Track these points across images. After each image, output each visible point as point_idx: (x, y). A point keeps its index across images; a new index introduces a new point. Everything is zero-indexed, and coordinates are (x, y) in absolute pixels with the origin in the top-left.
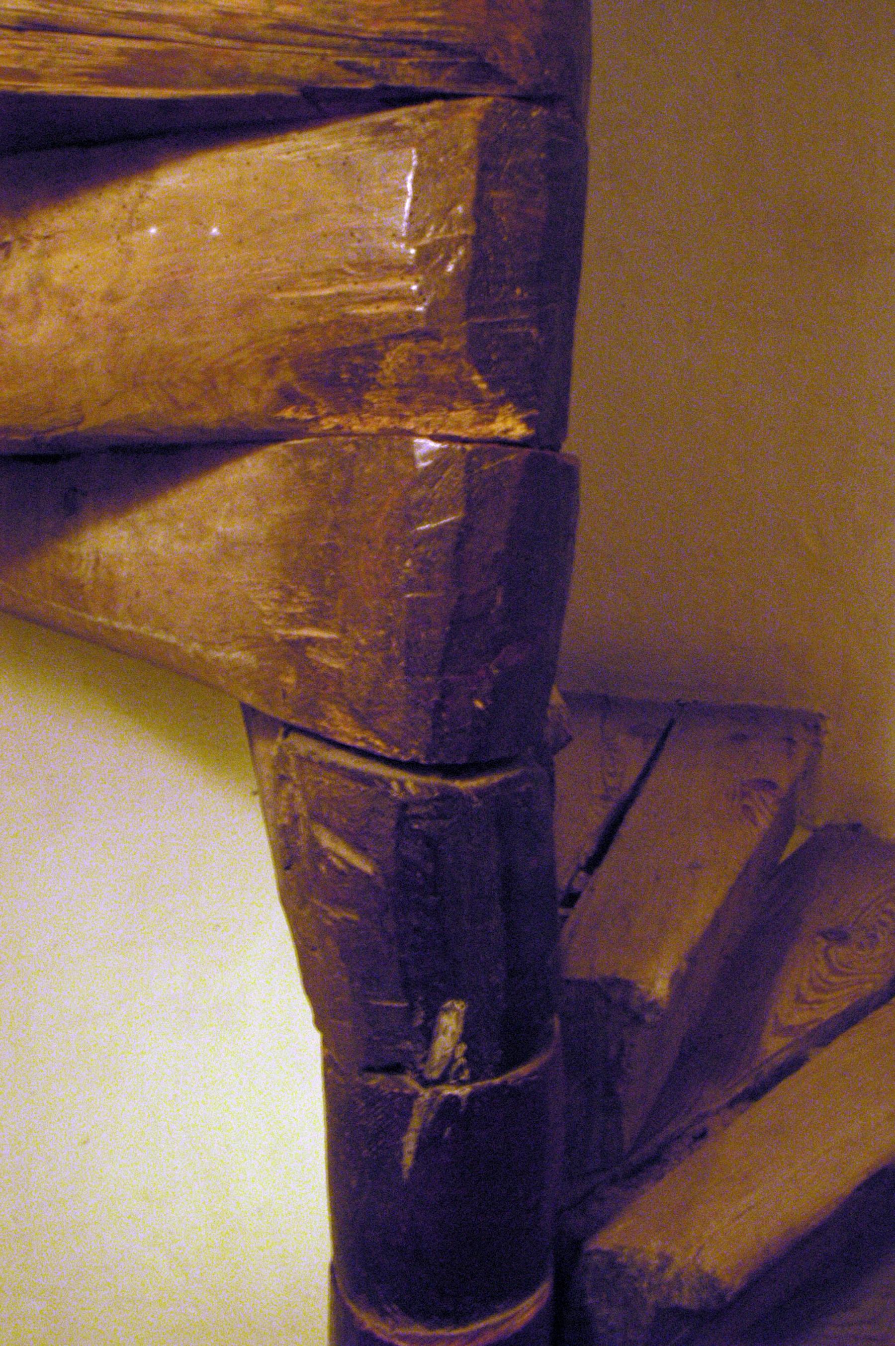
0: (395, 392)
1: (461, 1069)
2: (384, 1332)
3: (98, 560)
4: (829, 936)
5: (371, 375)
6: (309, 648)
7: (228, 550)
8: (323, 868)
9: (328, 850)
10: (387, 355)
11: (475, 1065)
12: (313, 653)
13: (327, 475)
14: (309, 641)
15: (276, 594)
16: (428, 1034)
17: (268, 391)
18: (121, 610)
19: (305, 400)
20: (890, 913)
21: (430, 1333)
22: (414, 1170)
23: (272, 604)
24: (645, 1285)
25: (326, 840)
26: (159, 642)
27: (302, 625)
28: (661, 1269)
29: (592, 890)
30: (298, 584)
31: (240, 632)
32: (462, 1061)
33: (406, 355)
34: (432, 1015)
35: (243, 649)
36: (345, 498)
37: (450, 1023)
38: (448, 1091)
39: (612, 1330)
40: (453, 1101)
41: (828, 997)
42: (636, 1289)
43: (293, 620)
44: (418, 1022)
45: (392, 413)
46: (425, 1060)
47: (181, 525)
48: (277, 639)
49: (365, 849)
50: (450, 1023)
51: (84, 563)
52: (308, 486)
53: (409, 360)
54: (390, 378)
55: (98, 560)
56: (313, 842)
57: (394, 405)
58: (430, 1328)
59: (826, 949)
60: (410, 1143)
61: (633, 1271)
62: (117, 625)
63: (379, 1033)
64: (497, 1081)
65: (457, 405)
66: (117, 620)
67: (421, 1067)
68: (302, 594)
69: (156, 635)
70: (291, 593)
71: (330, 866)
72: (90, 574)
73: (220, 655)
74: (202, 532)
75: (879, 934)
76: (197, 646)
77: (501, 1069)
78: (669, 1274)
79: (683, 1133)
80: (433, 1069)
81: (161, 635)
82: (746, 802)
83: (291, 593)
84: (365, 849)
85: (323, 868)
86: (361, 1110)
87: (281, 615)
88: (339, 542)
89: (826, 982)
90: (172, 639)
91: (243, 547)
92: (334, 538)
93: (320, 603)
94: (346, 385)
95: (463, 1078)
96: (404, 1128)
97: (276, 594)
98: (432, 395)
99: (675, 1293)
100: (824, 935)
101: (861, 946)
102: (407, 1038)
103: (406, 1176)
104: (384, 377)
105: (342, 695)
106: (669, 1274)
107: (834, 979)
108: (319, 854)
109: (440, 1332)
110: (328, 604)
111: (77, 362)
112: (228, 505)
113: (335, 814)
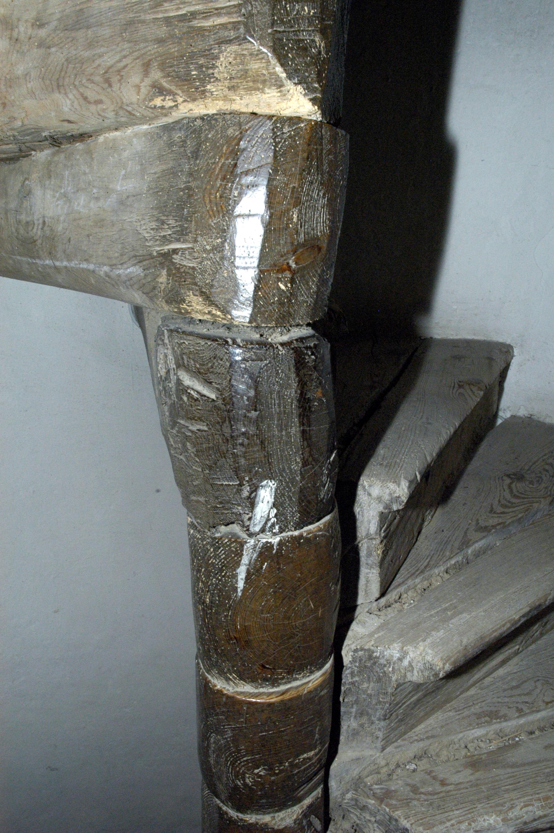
0: (227, 83)
1: (273, 525)
2: (228, 690)
3: (44, 223)
4: (512, 476)
5: (211, 71)
6: (174, 256)
7: (123, 203)
8: (185, 398)
9: (188, 387)
10: (221, 56)
11: (282, 521)
12: (177, 258)
13: (184, 142)
14: (175, 251)
15: (154, 225)
16: (252, 503)
17: (145, 86)
18: (60, 254)
19: (170, 92)
20: (551, 465)
21: (256, 691)
22: (245, 590)
23: (151, 232)
24: (391, 669)
25: (187, 380)
26: (83, 269)
27: (171, 242)
28: (400, 660)
29: (362, 435)
30: (167, 216)
31: (132, 253)
32: (274, 520)
33: (233, 56)
34: (255, 489)
35: (134, 265)
36: (196, 155)
37: (266, 495)
38: (265, 538)
39: (370, 696)
40: (268, 547)
41: (511, 510)
42: (385, 672)
43: (165, 240)
44: (245, 493)
45: (225, 98)
46: (250, 519)
47: (95, 191)
48: (155, 254)
49: (211, 383)
50: (266, 495)
51: (36, 227)
52: (172, 151)
53: (235, 59)
54: (223, 73)
55: (44, 223)
56: (179, 382)
57: (226, 92)
58: (257, 688)
59: (511, 483)
60: (242, 572)
61: (382, 661)
62: (58, 264)
63: (221, 503)
64: (296, 533)
65: (267, 90)
66: (58, 260)
67: (247, 523)
68: (170, 222)
69: (81, 266)
70: (163, 223)
71: (190, 396)
72: (39, 233)
73: (121, 271)
74: (108, 192)
75: (543, 476)
76: (106, 269)
77: (299, 526)
78: (406, 663)
79: (391, 494)
80: (255, 525)
81: (84, 266)
82: (461, 390)
83: (163, 223)
84: (211, 383)
85: (185, 398)
86: (211, 553)
87: (157, 238)
88: (193, 184)
89: (509, 502)
90: (91, 267)
91: (134, 198)
92: (189, 182)
93: (181, 226)
94: (194, 79)
95: (274, 531)
96: (238, 564)
97: (154, 225)
98: (251, 84)
99: (409, 674)
100: (508, 476)
101: (531, 483)
102: (239, 505)
103: (240, 594)
104: (219, 72)
105: (196, 284)
106: (406, 663)
107: (514, 500)
108: (182, 389)
109: (262, 690)
110: (186, 225)
111: (19, 72)
112: (123, 172)
113: (192, 362)
